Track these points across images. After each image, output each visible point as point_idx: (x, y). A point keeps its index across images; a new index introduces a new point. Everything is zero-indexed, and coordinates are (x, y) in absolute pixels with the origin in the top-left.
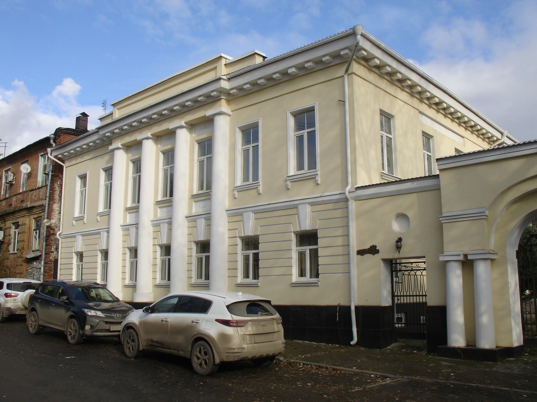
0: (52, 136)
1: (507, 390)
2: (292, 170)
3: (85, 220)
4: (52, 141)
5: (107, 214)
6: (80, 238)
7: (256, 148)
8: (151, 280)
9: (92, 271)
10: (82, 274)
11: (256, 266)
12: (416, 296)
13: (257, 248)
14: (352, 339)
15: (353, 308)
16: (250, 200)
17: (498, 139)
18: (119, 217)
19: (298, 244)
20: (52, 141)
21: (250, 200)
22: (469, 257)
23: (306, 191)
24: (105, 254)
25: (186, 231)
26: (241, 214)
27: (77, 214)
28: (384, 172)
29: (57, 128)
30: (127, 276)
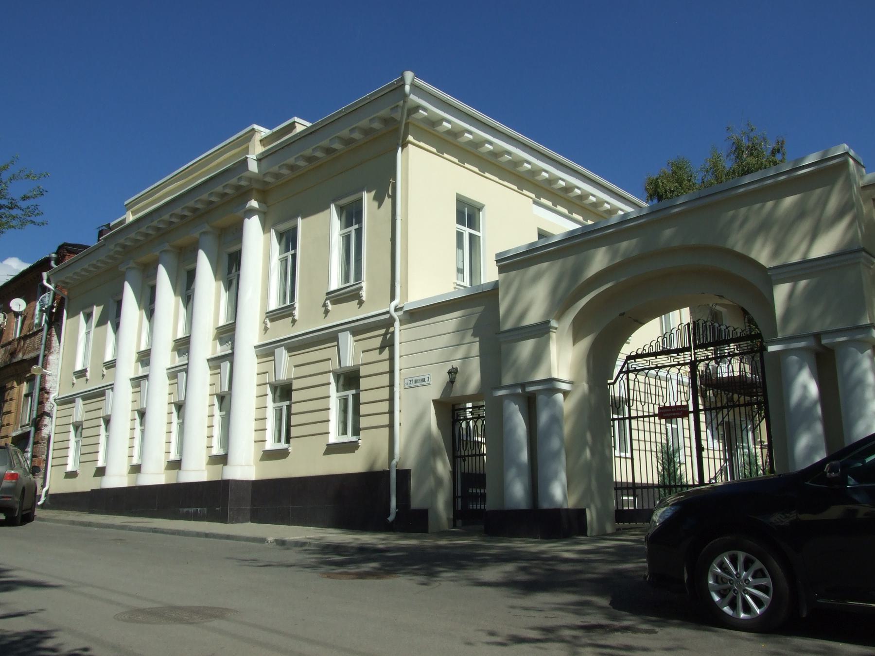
0: (54, 255)
4: (53, 263)
6: (80, 402)
8: (127, 458)
14: (389, 514)
15: (393, 475)
19: (277, 398)
20: (53, 263)
21: (283, 330)
23: (347, 313)
25: (167, 390)
26: (272, 354)
29: (61, 244)
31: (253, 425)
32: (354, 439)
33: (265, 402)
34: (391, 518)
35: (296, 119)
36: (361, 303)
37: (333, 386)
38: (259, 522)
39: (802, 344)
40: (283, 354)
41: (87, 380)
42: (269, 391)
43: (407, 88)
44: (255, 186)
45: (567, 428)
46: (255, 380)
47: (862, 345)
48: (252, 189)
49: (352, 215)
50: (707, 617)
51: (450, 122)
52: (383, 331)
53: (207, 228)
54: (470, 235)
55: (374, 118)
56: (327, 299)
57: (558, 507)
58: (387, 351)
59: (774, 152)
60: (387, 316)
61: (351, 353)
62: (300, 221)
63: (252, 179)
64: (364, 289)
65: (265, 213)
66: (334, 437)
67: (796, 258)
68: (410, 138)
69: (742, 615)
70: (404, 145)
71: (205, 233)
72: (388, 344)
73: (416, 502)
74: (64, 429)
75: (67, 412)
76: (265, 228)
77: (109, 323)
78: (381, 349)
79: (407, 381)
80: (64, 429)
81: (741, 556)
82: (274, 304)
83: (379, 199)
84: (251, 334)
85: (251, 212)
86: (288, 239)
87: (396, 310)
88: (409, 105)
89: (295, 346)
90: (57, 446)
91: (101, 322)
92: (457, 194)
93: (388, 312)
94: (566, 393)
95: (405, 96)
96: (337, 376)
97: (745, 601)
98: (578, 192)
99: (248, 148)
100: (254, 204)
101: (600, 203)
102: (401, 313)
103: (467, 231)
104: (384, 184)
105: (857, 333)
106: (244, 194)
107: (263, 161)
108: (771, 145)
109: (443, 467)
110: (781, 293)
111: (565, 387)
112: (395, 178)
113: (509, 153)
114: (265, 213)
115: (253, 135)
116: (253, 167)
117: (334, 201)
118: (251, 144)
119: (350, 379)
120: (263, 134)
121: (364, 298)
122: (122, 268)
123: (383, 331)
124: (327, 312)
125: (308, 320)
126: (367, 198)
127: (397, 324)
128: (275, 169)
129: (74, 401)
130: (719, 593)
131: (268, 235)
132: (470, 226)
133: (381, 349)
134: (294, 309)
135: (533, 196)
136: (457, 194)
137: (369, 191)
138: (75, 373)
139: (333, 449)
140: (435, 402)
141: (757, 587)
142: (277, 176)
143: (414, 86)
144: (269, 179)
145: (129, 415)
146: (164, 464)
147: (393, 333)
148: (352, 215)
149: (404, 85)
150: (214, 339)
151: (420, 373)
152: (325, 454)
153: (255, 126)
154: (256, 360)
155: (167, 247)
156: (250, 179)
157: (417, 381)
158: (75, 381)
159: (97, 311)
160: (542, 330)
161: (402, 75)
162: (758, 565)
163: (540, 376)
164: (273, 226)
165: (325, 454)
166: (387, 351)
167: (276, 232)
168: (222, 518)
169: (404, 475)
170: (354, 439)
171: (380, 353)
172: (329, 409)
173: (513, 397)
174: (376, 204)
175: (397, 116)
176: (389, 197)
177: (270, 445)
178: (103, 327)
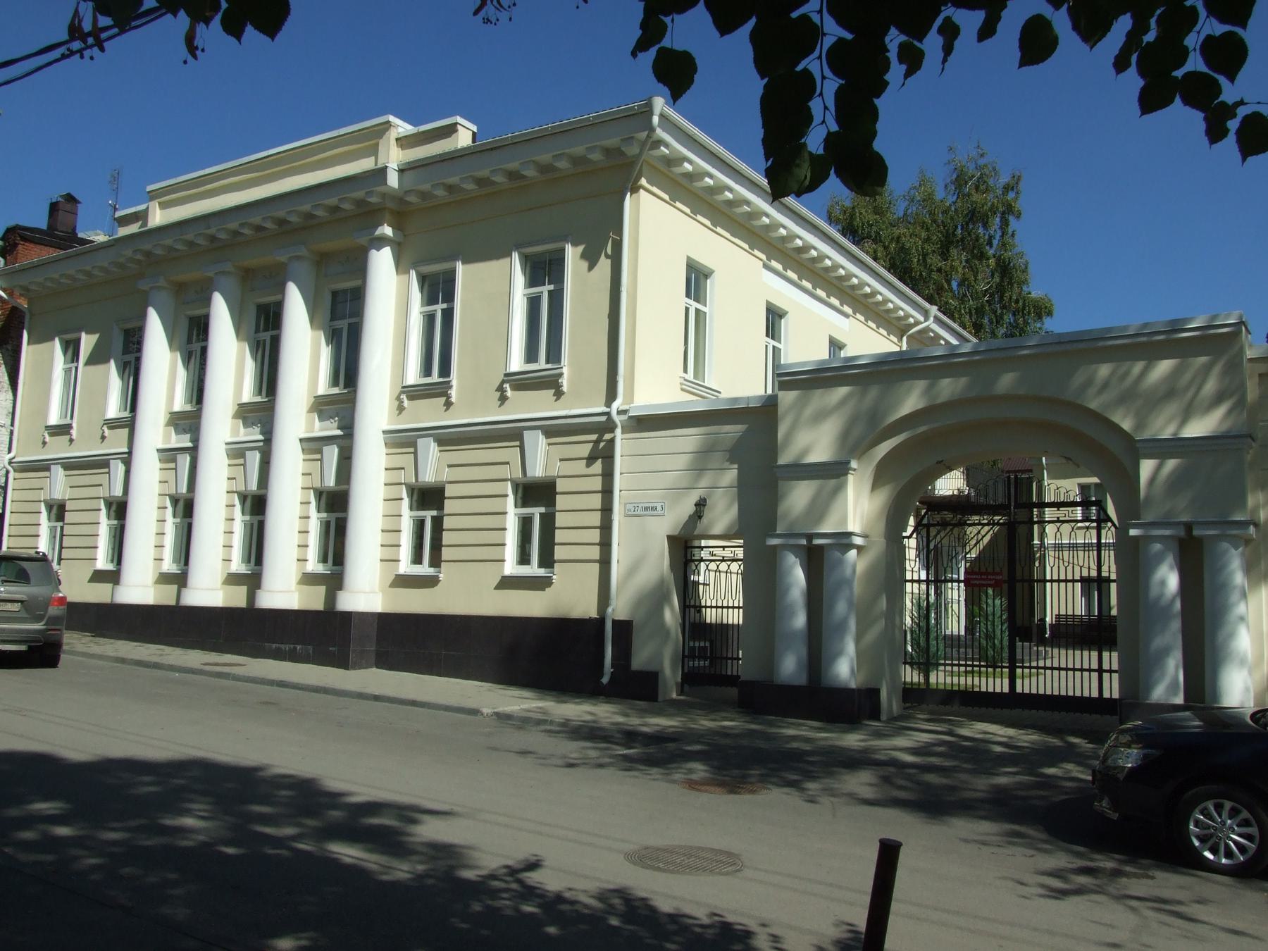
1: (724, 733)
2: (517, 363)
3: (74, 432)
5: (129, 424)
6: (58, 472)
7: (448, 315)
8: (151, 563)
9: (31, 530)
10: (61, 547)
11: (437, 546)
12: (717, 607)
13: (440, 507)
14: (602, 675)
16: (429, 414)
17: (917, 323)
18: (154, 432)
21: (429, 414)
22: (1196, 532)
23: (537, 405)
24: (119, 509)
27: (54, 419)
28: (687, 377)
29: (11, 223)
30: (168, 553)
31: (378, 538)
32: (542, 572)
33: (400, 508)
34: (605, 680)
35: (459, 120)
36: (559, 394)
37: (511, 500)
38: (390, 669)
39: (1167, 532)
40: (430, 449)
41: (71, 440)
42: (405, 495)
43: (656, 119)
44: (390, 205)
45: (857, 588)
46: (382, 477)
47: (1235, 541)
48: (384, 209)
49: (544, 270)
50: (1188, 861)
51: (694, 162)
52: (594, 437)
53: (303, 251)
54: (697, 310)
55: (595, 147)
56: (503, 382)
57: (843, 686)
58: (598, 467)
59: (1007, 188)
60: (603, 418)
61: (541, 459)
62: (460, 268)
63: (389, 195)
64: (565, 376)
65: (399, 244)
66: (511, 567)
67: (1167, 434)
68: (643, 181)
69: (1224, 861)
70: (635, 189)
71: (298, 258)
72: (603, 455)
73: (640, 659)
74: (29, 507)
75: (36, 483)
76: (401, 265)
77: (112, 363)
78: (591, 460)
79: (630, 507)
80: (29, 507)
81: (1228, 805)
82: (413, 376)
83: (591, 258)
84: (377, 410)
85: (380, 242)
86: (438, 289)
87: (619, 412)
88: (654, 138)
89: (449, 439)
90: (15, 531)
91: (97, 358)
92: (768, 302)
93: (608, 414)
94: (860, 549)
95: (652, 130)
96: (516, 486)
97: (1227, 846)
98: (766, 220)
99: (377, 145)
100: (387, 230)
101: (806, 248)
102: (624, 417)
103: (694, 305)
104: (604, 238)
105: (1234, 531)
106: (368, 215)
107: (406, 173)
108: (1004, 179)
109: (671, 616)
110: (1147, 467)
111: (858, 541)
112: (619, 230)
113: (748, 203)
114: (399, 244)
115: (387, 129)
116: (393, 180)
117: (517, 247)
118: (382, 142)
119: (537, 493)
120: (400, 130)
121: (565, 389)
122: (143, 285)
123: (594, 437)
124: (503, 399)
125: (471, 405)
126: (572, 254)
127: (618, 431)
128: (426, 187)
129: (47, 469)
130: (1198, 837)
131: (405, 277)
132: (697, 300)
133: (591, 460)
134: (451, 387)
135: (763, 257)
136: (768, 302)
137: (575, 244)
138: (48, 428)
139: (508, 583)
140: (669, 537)
141: (1239, 835)
142: (424, 195)
143: (662, 116)
144: (412, 199)
145: (155, 501)
146: (220, 578)
147: (612, 441)
148: (544, 270)
149: (652, 114)
150: (311, 410)
151: (653, 498)
152: (497, 588)
153: (392, 118)
154: (384, 450)
155: (229, 267)
156: (384, 195)
157: (645, 509)
158: (48, 439)
159: (87, 342)
160: (835, 471)
161: (650, 99)
162: (1245, 814)
163: (826, 528)
164: (415, 265)
165: (497, 588)
166: (598, 467)
167: (418, 274)
168: (342, 662)
169: (624, 629)
170: (542, 572)
171: (588, 465)
172: (505, 529)
173: (795, 549)
174: (585, 265)
175: (632, 150)
176: (607, 256)
177: (405, 566)
178: (101, 368)
